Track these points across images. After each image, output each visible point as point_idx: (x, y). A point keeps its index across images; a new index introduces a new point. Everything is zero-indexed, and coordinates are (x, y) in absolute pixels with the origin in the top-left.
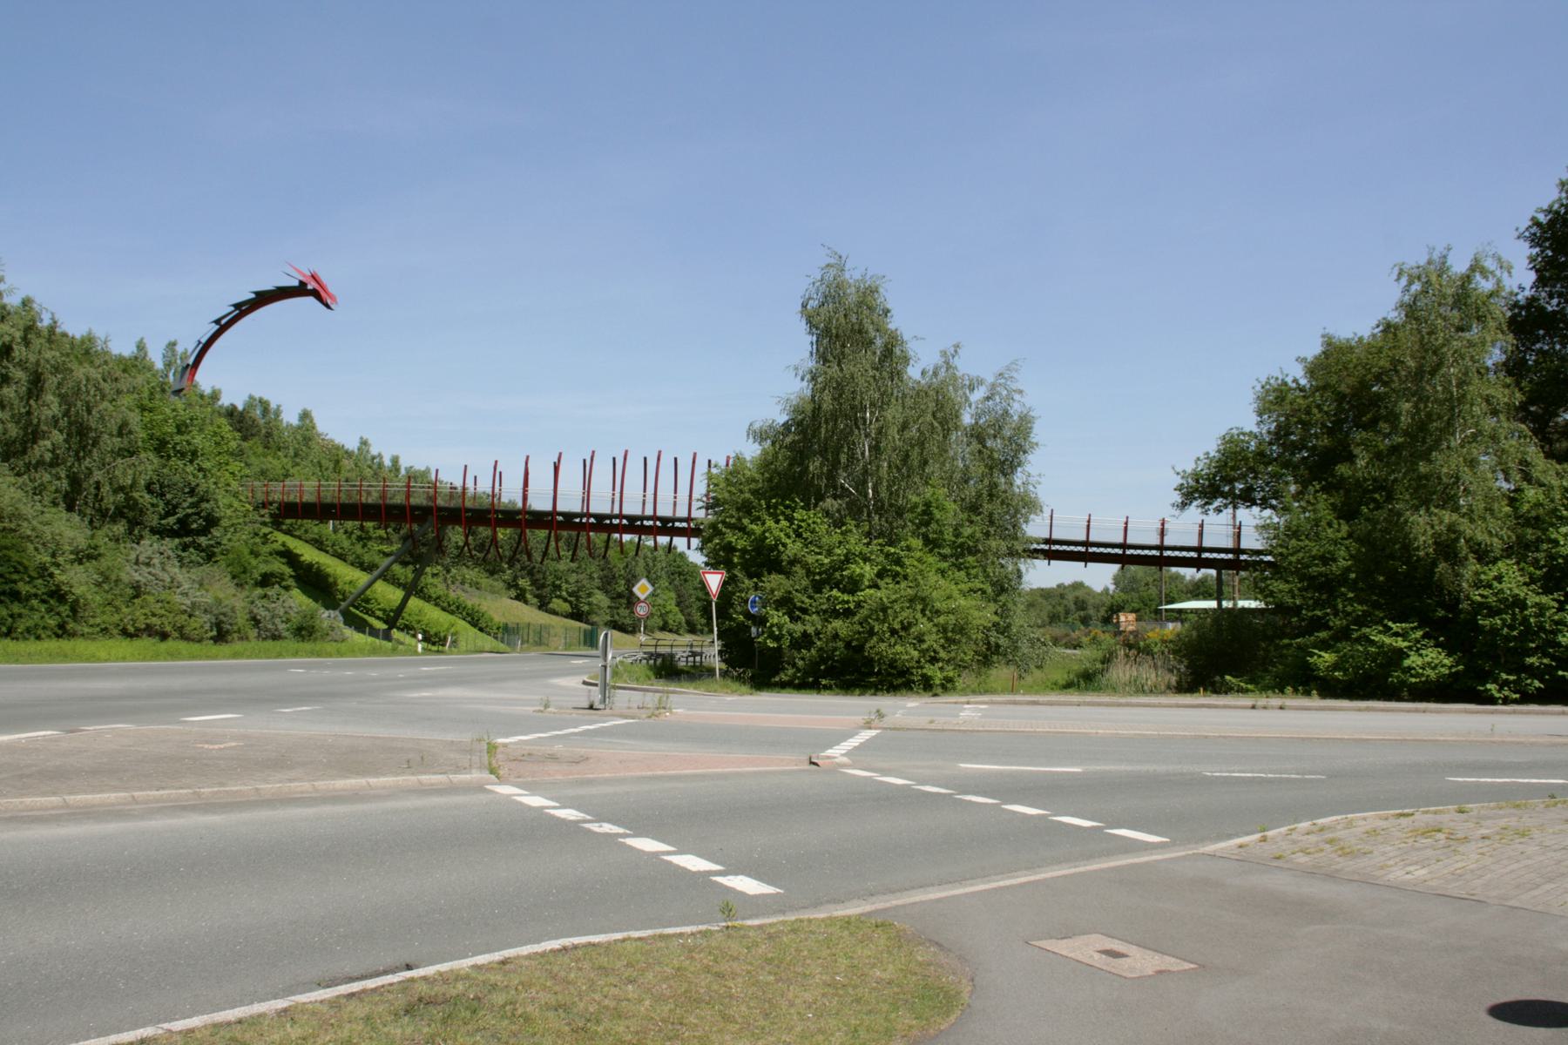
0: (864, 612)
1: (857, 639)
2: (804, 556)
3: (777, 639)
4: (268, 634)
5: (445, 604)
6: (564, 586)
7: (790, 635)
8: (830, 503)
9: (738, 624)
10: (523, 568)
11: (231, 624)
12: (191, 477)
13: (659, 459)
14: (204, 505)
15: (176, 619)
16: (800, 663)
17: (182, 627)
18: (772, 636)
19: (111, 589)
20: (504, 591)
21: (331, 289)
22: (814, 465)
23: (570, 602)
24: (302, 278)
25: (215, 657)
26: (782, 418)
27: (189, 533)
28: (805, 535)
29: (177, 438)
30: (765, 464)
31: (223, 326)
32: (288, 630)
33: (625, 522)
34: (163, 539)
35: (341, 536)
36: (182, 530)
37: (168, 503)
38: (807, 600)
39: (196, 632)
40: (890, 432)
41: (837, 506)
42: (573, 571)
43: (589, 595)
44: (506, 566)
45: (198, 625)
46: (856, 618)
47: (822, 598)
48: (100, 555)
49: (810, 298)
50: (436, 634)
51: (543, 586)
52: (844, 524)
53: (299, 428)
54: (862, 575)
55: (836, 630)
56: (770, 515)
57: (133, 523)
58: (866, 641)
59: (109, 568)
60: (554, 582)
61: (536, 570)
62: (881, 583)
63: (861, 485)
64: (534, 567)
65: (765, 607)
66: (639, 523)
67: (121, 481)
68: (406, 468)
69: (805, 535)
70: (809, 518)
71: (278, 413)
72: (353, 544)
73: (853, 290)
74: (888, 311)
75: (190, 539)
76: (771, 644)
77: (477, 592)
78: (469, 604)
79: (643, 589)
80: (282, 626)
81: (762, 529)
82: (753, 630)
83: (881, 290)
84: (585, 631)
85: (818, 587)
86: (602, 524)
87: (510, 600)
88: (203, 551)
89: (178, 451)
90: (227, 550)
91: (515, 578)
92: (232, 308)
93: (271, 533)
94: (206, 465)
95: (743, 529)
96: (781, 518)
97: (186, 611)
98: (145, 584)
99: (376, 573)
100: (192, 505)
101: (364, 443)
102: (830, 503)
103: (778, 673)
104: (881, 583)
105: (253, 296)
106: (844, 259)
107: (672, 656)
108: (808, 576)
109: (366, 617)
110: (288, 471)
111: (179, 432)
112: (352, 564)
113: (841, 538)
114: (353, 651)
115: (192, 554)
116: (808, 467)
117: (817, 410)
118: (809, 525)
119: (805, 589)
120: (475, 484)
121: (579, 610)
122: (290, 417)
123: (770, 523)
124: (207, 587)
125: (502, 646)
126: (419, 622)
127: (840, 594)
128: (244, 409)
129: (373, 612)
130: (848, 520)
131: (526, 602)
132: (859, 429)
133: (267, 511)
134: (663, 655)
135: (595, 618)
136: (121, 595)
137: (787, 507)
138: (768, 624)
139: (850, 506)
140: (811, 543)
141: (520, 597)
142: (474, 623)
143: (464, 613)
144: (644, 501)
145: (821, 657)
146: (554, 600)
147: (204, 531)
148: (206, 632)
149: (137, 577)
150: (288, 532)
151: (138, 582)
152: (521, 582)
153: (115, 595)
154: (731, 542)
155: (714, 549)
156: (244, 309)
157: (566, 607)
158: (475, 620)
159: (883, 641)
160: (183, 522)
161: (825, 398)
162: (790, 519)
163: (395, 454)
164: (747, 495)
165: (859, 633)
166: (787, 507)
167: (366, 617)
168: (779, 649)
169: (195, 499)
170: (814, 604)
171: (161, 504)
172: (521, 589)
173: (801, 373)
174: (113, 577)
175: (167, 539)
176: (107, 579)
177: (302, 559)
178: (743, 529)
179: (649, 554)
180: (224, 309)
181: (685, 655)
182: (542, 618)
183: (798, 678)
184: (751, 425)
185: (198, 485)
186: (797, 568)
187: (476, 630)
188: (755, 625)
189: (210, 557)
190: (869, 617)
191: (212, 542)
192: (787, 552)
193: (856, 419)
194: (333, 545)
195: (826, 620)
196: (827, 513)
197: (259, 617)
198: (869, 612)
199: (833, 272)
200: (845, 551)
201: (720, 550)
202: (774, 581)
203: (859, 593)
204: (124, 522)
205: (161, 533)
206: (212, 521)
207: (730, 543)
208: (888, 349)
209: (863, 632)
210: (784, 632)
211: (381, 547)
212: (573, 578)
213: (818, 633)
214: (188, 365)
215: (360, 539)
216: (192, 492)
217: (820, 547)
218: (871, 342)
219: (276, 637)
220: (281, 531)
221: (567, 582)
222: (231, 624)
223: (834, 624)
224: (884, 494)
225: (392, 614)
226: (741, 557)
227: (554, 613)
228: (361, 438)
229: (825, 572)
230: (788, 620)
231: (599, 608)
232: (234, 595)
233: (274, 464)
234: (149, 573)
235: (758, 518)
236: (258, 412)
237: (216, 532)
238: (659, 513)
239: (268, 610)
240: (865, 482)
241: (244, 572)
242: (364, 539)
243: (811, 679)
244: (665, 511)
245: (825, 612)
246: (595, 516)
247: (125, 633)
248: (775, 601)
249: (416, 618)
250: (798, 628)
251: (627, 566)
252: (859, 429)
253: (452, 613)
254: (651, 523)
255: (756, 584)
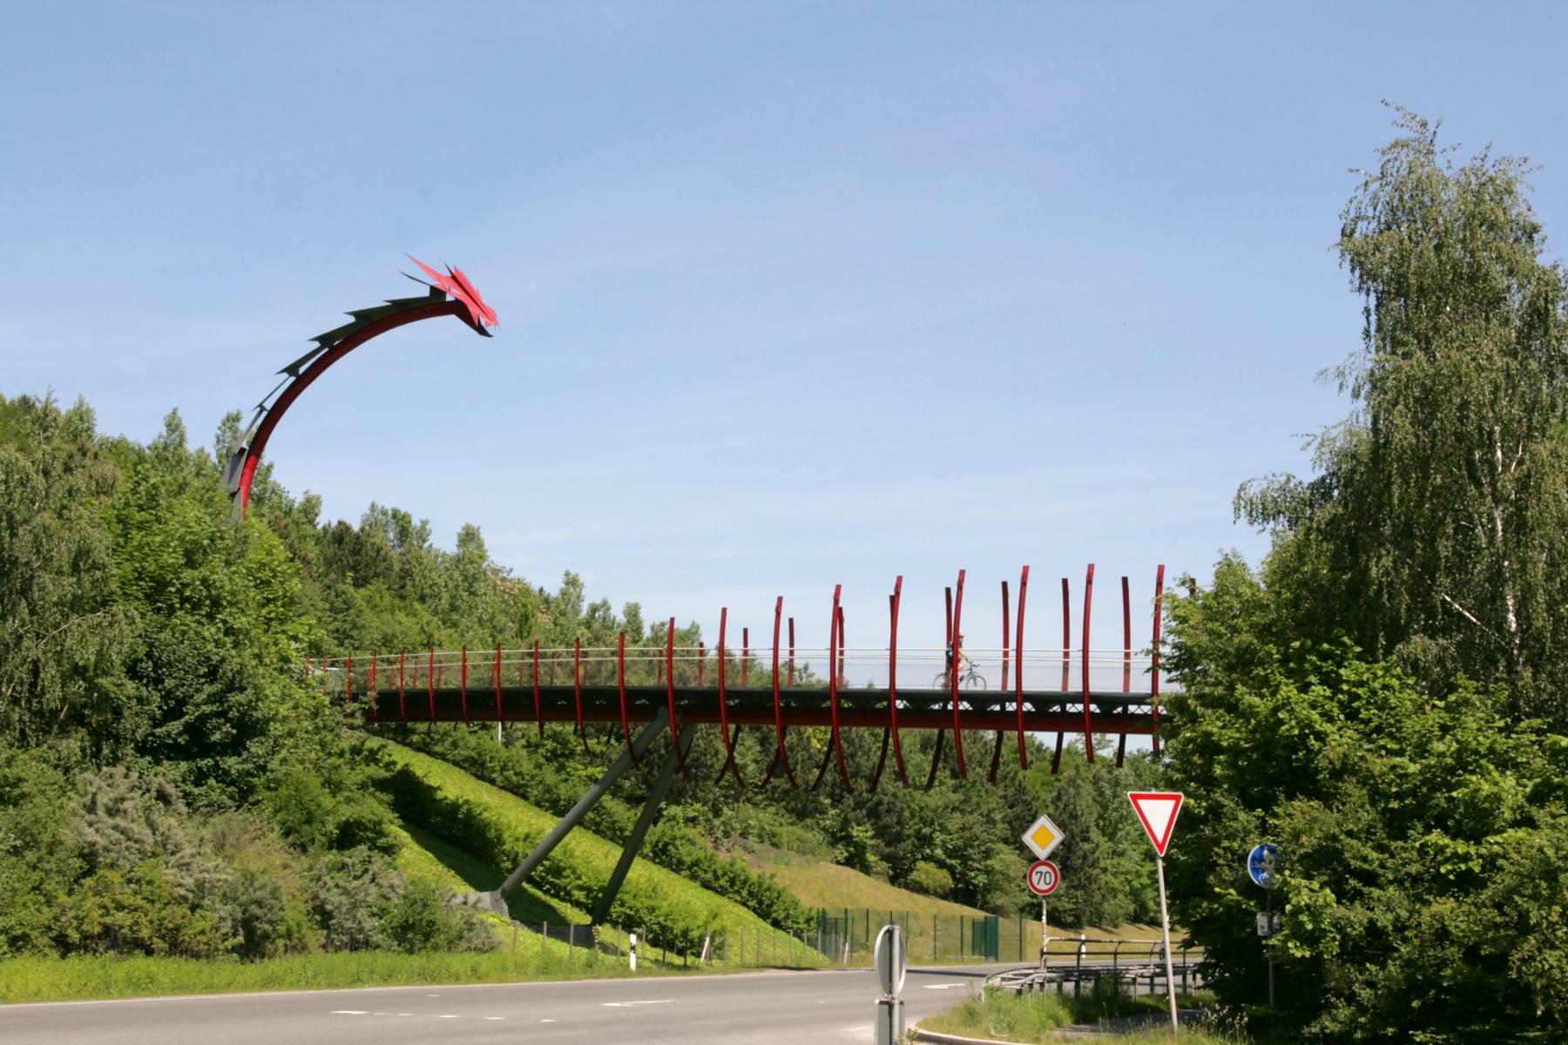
0: (1502, 881)
1: (1493, 941)
2: (1362, 758)
3: (1311, 939)
4: (345, 939)
5: (709, 876)
6: (939, 838)
7: (1340, 930)
8: (1418, 645)
9: (1228, 908)
10: (859, 805)
11: (271, 922)
12: (210, 646)
13: (1089, 582)
14: (235, 698)
15: (164, 913)
16: (1365, 994)
17: (177, 929)
18: (1299, 934)
19: (40, 860)
20: (825, 848)
21: (486, 299)
22: (1380, 566)
23: (951, 869)
24: (435, 283)
25: (228, 986)
26: (1308, 473)
27: (208, 750)
28: (1363, 714)
29: (187, 575)
30: (1285, 570)
31: (302, 377)
32: (383, 931)
33: (1028, 706)
34: (158, 762)
35: (518, 751)
36: (196, 744)
37: (167, 695)
38: (1374, 855)
39: (203, 939)
40: (1548, 484)
41: (1435, 650)
42: (954, 809)
43: (988, 854)
44: (827, 801)
45: (206, 925)
46: (1485, 895)
47: (1406, 855)
48: (23, 796)
49: (1358, 218)
50: (685, 933)
51: (898, 838)
52: (1453, 688)
53: (459, 560)
54: (1496, 799)
55: (1441, 920)
56: (1289, 674)
57: (99, 735)
58: (1513, 944)
59: (37, 821)
60: (919, 831)
61: (882, 808)
62: (1540, 815)
63: (1490, 606)
64: (880, 803)
65: (1280, 871)
66: (1057, 708)
67: (77, 658)
68: (653, 628)
69: (1363, 714)
70: (1375, 675)
71: (423, 535)
72: (539, 766)
73: (1453, 192)
74: (1535, 229)
75: (210, 762)
76: (1298, 951)
77: (773, 853)
78: (754, 874)
79: (1044, 837)
80: (371, 924)
81: (1271, 705)
82: (1261, 920)
83: (1517, 188)
84: (974, 924)
85: (1397, 825)
86: (984, 709)
87: (834, 866)
88: (233, 783)
89: (188, 599)
90: (275, 780)
91: (845, 823)
92: (317, 345)
93: (384, 746)
94: (241, 622)
95: (1232, 708)
96: (1313, 679)
97: (185, 898)
98: (106, 849)
99: (569, 816)
100: (212, 699)
101: (572, 582)
102: (1418, 645)
103: (1315, 1016)
104: (1540, 815)
105: (352, 319)
106: (1431, 127)
107: (1116, 975)
108: (1373, 803)
109: (554, 902)
110: (431, 636)
111: (191, 563)
112: (538, 804)
113: (1446, 718)
114: (505, 969)
115: (214, 790)
116: (1368, 569)
117: (1380, 449)
118: (1374, 693)
119: (1369, 831)
120: (746, 644)
121: (968, 883)
122: (444, 542)
123: (1288, 690)
124: (229, 851)
125: (813, 955)
126: (652, 910)
127: (1447, 841)
128: (362, 530)
129: (568, 893)
130: (1461, 678)
131: (866, 869)
132: (1479, 485)
133: (357, 705)
134: (1096, 973)
135: (998, 899)
136: (59, 872)
137: (1325, 656)
138: (1288, 908)
139: (1465, 648)
140: (1379, 729)
141: (856, 860)
142: (763, 912)
143: (744, 893)
144: (1066, 664)
145: (1410, 979)
146: (921, 864)
147: (235, 746)
148: (225, 937)
149: (90, 835)
150: (424, 748)
151: (93, 844)
152: (857, 832)
153: (47, 872)
154: (1210, 734)
155: (1183, 751)
156: (336, 345)
157: (943, 878)
158: (765, 905)
159: (1553, 947)
160: (196, 730)
161: (1398, 421)
162: (1332, 682)
163: (632, 601)
164: (1246, 638)
165: (1496, 926)
166: (1325, 656)
167: (554, 902)
168: (1317, 960)
169: (216, 687)
170: (1389, 863)
171: (156, 697)
172: (856, 845)
173: (1351, 382)
174: (46, 838)
175: (166, 763)
176: (31, 843)
177: (439, 795)
178: (1232, 708)
179: (1104, 772)
180: (303, 346)
181: (1146, 972)
182: (898, 899)
183: (1363, 1027)
184: (1242, 488)
185: (223, 660)
186: (1350, 787)
187: (767, 927)
188: (1263, 909)
189: (244, 794)
190: (1515, 890)
191: (249, 766)
192: (1327, 751)
193: (1470, 464)
194: (503, 769)
195: (1419, 899)
196: (1414, 666)
197: (329, 907)
198: (1515, 881)
199: (1405, 157)
200: (1455, 746)
201: (1193, 753)
202: (1298, 812)
203: (1491, 839)
204: (83, 732)
205: (155, 750)
206: (248, 728)
207: (1209, 735)
208: (1537, 311)
209: (1506, 926)
210: (1325, 925)
211: (590, 770)
212: (953, 823)
213: (1400, 927)
214: (242, 450)
215: (553, 756)
216: (212, 675)
217: (1399, 741)
218: (1498, 300)
219: (357, 944)
220: (410, 745)
221: (943, 829)
222: (271, 922)
223: (1435, 908)
224: (1541, 620)
225: (601, 895)
226: (1232, 765)
227: (920, 889)
228: (567, 574)
229: (1413, 792)
230: (1332, 897)
231: (1008, 879)
232: (285, 866)
233: (406, 624)
234: (115, 828)
235: (1265, 681)
236: (391, 535)
237: (256, 747)
238: (1095, 688)
239: (346, 892)
240: (1497, 597)
241: (309, 821)
242: (562, 756)
243: (1390, 1031)
244: (1106, 682)
245: (1416, 879)
246: (1033, 698)
247: (64, 946)
248: (1302, 858)
249: (648, 903)
250: (1357, 915)
251: (1059, 798)
252: (1479, 485)
253: (722, 892)
254: (1080, 707)
255: (1264, 822)
